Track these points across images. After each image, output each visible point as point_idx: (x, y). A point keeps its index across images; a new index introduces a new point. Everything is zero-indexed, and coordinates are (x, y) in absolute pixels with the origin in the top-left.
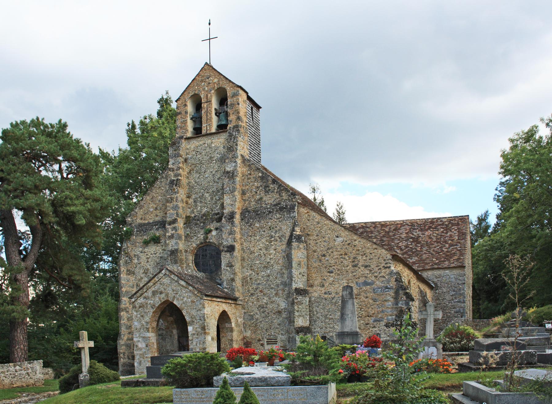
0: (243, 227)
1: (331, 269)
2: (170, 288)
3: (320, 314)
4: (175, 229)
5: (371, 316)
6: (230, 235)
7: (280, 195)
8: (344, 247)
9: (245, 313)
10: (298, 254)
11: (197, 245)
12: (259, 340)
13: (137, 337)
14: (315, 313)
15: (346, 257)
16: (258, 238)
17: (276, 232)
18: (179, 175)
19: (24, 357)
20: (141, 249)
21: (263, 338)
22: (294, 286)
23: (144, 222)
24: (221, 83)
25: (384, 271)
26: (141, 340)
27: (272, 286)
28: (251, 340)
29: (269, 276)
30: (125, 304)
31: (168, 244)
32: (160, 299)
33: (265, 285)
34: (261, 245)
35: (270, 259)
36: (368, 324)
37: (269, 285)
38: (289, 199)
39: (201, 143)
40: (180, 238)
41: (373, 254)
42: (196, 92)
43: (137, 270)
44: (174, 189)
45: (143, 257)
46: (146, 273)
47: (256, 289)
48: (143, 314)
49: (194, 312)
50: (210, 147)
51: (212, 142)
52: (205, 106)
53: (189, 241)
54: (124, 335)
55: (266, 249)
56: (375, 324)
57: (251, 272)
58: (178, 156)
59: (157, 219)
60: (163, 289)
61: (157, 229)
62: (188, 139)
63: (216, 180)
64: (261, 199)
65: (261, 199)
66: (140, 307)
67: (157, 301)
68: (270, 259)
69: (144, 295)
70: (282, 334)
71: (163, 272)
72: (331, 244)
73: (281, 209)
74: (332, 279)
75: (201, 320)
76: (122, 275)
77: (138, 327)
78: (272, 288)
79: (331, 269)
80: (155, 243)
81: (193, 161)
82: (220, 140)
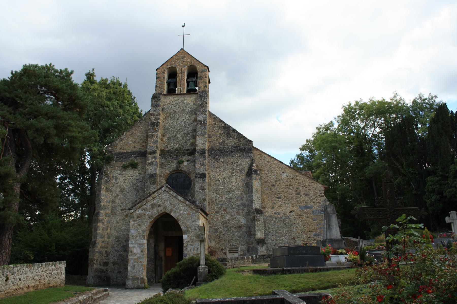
0: (210, 161)
1: (279, 195)
2: (168, 203)
3: (271, 229)
4: (155, 157)
5: (312, 231)
6: (202, 165)
7: (239, 140)
8: (289, 180)
9: (210, 227)
10: (256, 184)
11: (170, 171)
12: (222, 250)
13: (133, 244)
14: (267, 228)
15: (291, 187)
16: (222, 169)
17: (237, 166)
18: (159, 119)
19: (7, 262)
20: (119, 172)
21: (225, 248)
22: (254, 206)
23: (122, 151)
24: (193, 62)
25: (319, 198)
26: (136, 246)
27: (234, 206)
28: (215, 249)
29: (231, 198)
30: (102, 216)
31: (148, 169)
32: (158, 211)
33: (228, 205)
34: (225, 175)
35: (232, 186)
36: (310, 237)
37: (232, 206)
38: (246, 144)
39: (176, 99)
40: (156, 165)
41: (311, 186)
42: (173, 66)
43: (114, 188)
44: (155, 129)
45: (121, 179)
46: (122, 192)
47: (221, 208)
48: (140, 223)
49: (189, 223)
50: (183, 103)
51: (185, 100)
52: (180, 75)
53: (163, 168)
54: (99, 243)
55: (229, 179)
56: (315, 237)
57: (216, 195)
58: (159, 106)
59: (135, 150)
60: (161, 203)
61: (136, 157)
62: (164, 95)
63: (187, 125)
64: (224, 142)
65: (224, 142)
66: (138, 217)
67: (155, 212)
68: (232, 186)
69: (143, 207)
70: (242, 245)
71: (163, 189)
72: (279, 178)
73: (241, 150)
74: (280, 203)
75: (195, 229)
76: (102, 192)
77: (135, 235)
78: (234, 208)
79: (279, 195)
80: (132, 168)
81: (168, 111)
82: (191, 99)
